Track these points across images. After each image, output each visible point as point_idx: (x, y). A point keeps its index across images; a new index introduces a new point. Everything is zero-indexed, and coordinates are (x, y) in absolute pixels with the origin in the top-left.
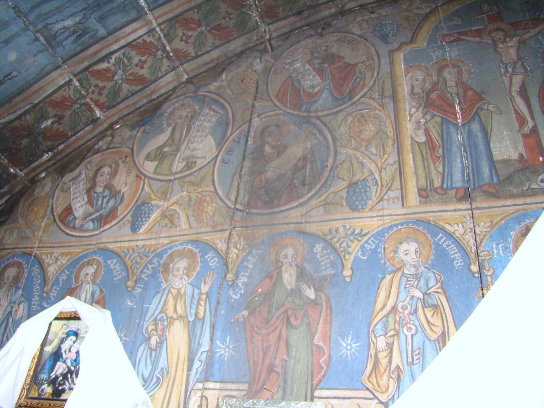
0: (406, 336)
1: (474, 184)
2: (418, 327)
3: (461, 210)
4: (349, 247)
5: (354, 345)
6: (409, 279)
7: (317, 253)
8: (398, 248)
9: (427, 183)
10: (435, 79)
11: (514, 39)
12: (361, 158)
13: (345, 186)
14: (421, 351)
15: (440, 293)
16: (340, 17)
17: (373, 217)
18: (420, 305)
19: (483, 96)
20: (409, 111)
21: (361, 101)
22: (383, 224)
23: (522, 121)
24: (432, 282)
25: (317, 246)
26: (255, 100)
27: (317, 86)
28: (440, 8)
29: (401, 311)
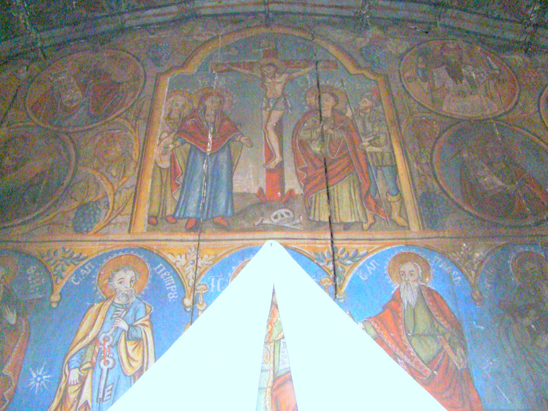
0: (102, 370)
1: (207, 215)
2: (117, 361)
3: (188, 241)
4: (63, 270)
5: (44, 377)
6: (118, 309)
7: (29, 275)
8: (113, 276)
9: (159, 210)
10: (196, 105)
11: (284, 75)
12: (99, 179)
13: (75, 206)
14: (115, 386)
15: (147, 326)
16: (120, 34)
17: (96, 241)
18: (123, 337)
19: (238, 127)
20: (161, 135)
21: (116, 120)
22: (105, 249)
23: (270, 155)
24: (141, 314)
25: (32, 267)
26: (9, 108)
27: (76, 101)
28: (220, 38)
29: (102, 342)
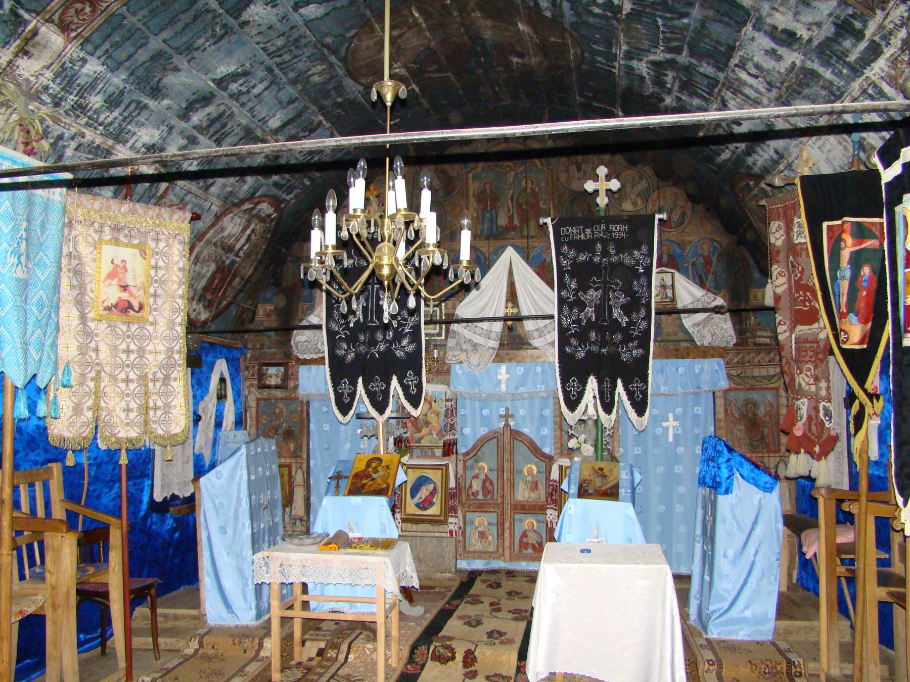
23: (509, 211)
